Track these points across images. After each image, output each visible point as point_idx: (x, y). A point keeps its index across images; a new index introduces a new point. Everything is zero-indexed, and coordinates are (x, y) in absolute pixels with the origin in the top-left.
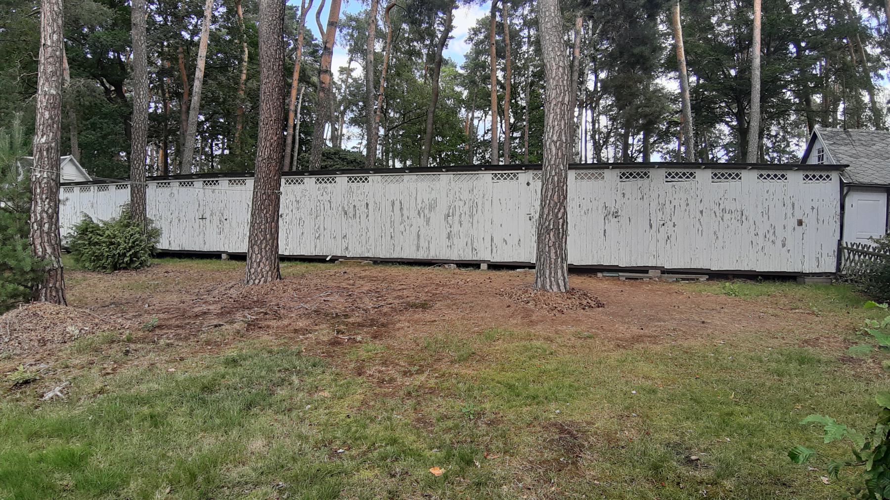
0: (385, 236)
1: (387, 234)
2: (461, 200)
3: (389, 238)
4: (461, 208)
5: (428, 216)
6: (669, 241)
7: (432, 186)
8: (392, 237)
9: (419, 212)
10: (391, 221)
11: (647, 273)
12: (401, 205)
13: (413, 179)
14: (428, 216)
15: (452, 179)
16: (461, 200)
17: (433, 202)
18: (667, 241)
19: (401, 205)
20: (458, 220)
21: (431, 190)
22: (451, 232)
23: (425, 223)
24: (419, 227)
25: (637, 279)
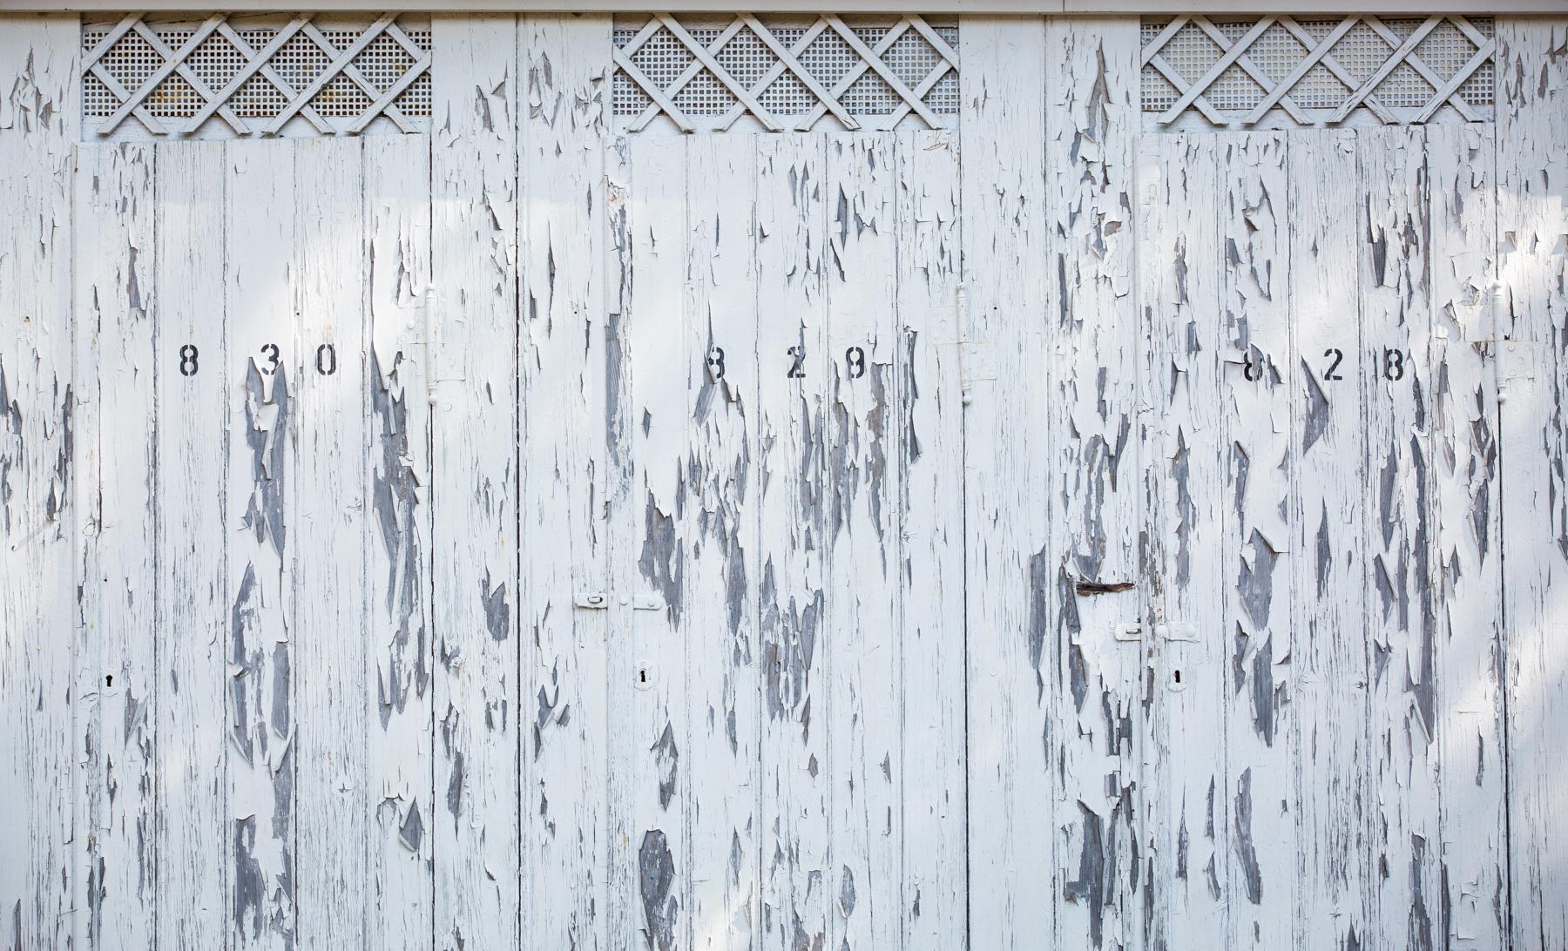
0: (150, 871)
1: (173, 851)
2: (1252, 367)
3: (213, 902)
4: (1264, 485)
5: (793, 590)
6: (1074, 210)
7: (843, 172)
8: (248, 886)
9: (660, 529)
10: (243, 662)
11: (776, 646)
12: (395, 440)
13: (571, 77)
14: (793, 590)
15: (1126, 80)
16: (1252, 367)
17: (859, 399)
18: (1079, 211)
19: (395, 440)
20: (1220, 645)
21: (821, 219)
22: (1125, 800)
23: (750, 678)
24: (666, 742)
25: (1510, 917)
